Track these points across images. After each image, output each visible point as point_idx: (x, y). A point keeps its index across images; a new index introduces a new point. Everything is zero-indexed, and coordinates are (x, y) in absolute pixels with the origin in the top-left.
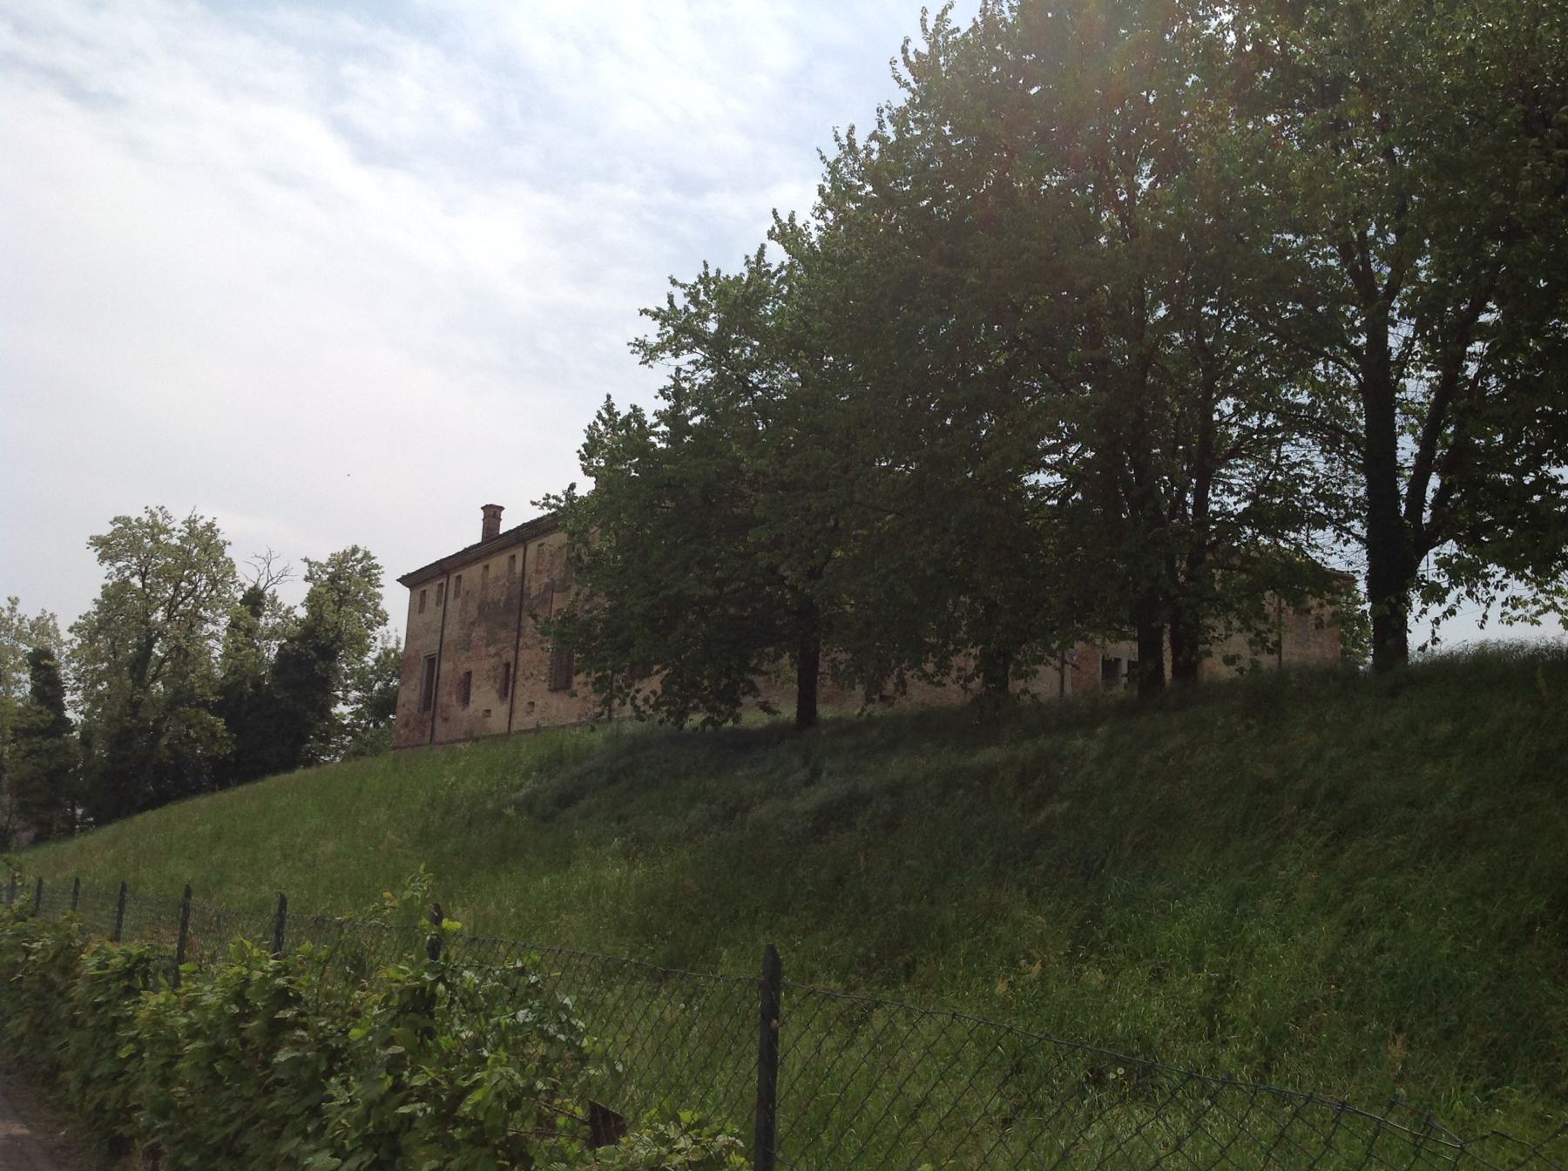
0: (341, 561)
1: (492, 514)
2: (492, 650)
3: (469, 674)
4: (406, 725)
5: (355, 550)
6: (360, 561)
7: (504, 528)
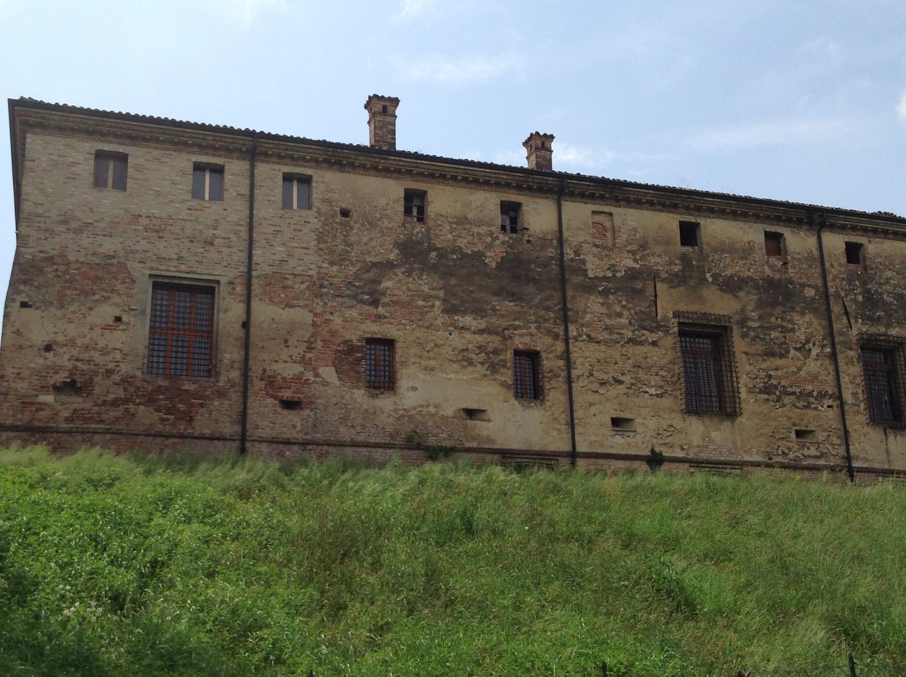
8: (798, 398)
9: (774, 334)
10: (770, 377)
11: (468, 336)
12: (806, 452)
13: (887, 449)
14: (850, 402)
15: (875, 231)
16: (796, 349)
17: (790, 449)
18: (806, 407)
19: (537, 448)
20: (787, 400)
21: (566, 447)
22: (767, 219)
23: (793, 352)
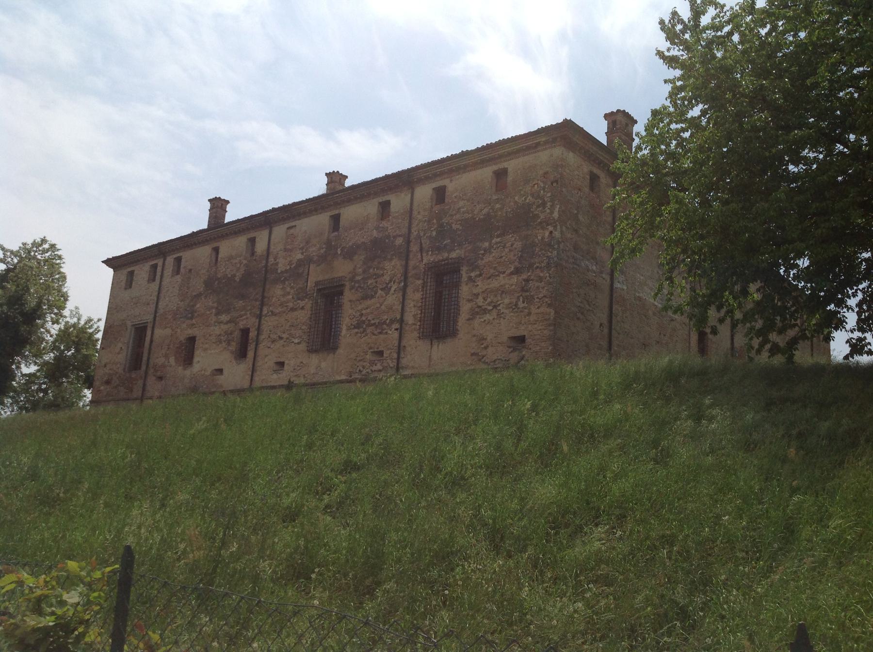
0: (27, 252)
1: (218, 206)
2: (224, 317)
3: (192, 340)
4: (108, 382)
5: (44, 241)
6: (45, 251)
7: (229, 217)
8: (376, 327)
9: (370, 282)
10: (362, 315)
11: (223, 326)
12: (375, 368)
13: (430, 356)
14: (410, 322)
15: (451, 171)
16: (382, 289)
17: (364, 367)
18: (380, 333)
19: (239, 387)
20: (369, 330)
21: (246, 384)
22: (376, 194)
23: (380, 292)
